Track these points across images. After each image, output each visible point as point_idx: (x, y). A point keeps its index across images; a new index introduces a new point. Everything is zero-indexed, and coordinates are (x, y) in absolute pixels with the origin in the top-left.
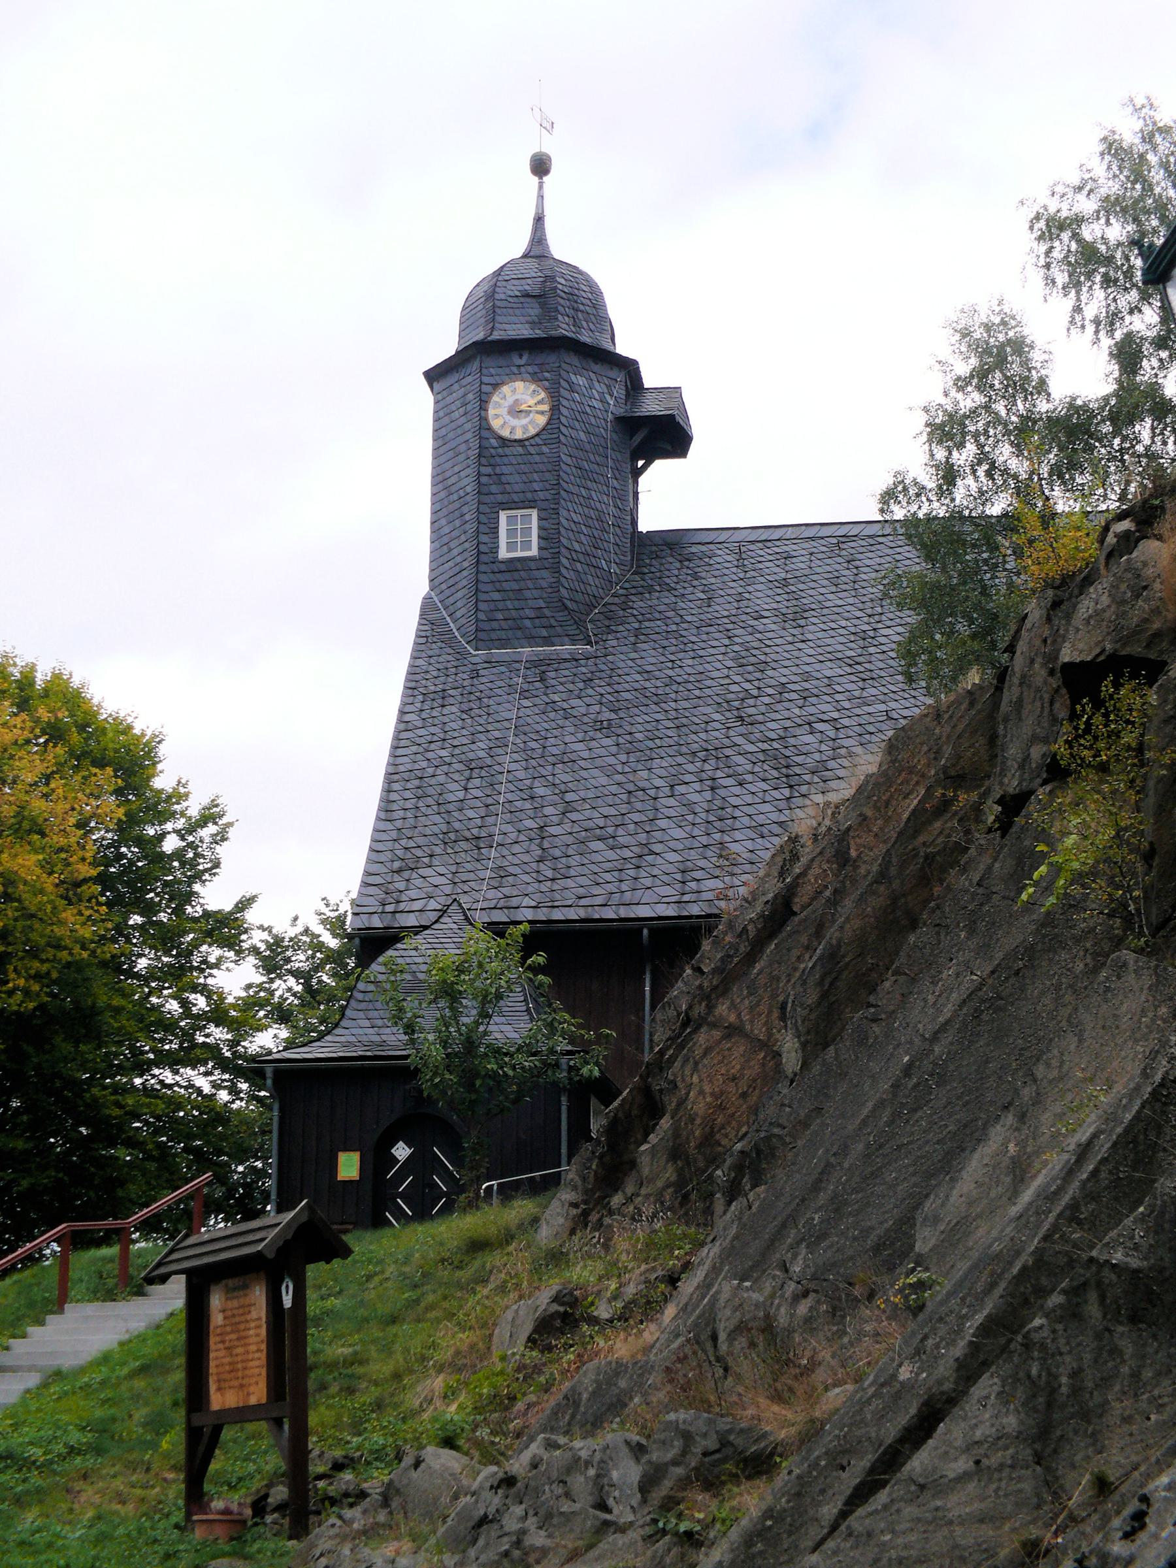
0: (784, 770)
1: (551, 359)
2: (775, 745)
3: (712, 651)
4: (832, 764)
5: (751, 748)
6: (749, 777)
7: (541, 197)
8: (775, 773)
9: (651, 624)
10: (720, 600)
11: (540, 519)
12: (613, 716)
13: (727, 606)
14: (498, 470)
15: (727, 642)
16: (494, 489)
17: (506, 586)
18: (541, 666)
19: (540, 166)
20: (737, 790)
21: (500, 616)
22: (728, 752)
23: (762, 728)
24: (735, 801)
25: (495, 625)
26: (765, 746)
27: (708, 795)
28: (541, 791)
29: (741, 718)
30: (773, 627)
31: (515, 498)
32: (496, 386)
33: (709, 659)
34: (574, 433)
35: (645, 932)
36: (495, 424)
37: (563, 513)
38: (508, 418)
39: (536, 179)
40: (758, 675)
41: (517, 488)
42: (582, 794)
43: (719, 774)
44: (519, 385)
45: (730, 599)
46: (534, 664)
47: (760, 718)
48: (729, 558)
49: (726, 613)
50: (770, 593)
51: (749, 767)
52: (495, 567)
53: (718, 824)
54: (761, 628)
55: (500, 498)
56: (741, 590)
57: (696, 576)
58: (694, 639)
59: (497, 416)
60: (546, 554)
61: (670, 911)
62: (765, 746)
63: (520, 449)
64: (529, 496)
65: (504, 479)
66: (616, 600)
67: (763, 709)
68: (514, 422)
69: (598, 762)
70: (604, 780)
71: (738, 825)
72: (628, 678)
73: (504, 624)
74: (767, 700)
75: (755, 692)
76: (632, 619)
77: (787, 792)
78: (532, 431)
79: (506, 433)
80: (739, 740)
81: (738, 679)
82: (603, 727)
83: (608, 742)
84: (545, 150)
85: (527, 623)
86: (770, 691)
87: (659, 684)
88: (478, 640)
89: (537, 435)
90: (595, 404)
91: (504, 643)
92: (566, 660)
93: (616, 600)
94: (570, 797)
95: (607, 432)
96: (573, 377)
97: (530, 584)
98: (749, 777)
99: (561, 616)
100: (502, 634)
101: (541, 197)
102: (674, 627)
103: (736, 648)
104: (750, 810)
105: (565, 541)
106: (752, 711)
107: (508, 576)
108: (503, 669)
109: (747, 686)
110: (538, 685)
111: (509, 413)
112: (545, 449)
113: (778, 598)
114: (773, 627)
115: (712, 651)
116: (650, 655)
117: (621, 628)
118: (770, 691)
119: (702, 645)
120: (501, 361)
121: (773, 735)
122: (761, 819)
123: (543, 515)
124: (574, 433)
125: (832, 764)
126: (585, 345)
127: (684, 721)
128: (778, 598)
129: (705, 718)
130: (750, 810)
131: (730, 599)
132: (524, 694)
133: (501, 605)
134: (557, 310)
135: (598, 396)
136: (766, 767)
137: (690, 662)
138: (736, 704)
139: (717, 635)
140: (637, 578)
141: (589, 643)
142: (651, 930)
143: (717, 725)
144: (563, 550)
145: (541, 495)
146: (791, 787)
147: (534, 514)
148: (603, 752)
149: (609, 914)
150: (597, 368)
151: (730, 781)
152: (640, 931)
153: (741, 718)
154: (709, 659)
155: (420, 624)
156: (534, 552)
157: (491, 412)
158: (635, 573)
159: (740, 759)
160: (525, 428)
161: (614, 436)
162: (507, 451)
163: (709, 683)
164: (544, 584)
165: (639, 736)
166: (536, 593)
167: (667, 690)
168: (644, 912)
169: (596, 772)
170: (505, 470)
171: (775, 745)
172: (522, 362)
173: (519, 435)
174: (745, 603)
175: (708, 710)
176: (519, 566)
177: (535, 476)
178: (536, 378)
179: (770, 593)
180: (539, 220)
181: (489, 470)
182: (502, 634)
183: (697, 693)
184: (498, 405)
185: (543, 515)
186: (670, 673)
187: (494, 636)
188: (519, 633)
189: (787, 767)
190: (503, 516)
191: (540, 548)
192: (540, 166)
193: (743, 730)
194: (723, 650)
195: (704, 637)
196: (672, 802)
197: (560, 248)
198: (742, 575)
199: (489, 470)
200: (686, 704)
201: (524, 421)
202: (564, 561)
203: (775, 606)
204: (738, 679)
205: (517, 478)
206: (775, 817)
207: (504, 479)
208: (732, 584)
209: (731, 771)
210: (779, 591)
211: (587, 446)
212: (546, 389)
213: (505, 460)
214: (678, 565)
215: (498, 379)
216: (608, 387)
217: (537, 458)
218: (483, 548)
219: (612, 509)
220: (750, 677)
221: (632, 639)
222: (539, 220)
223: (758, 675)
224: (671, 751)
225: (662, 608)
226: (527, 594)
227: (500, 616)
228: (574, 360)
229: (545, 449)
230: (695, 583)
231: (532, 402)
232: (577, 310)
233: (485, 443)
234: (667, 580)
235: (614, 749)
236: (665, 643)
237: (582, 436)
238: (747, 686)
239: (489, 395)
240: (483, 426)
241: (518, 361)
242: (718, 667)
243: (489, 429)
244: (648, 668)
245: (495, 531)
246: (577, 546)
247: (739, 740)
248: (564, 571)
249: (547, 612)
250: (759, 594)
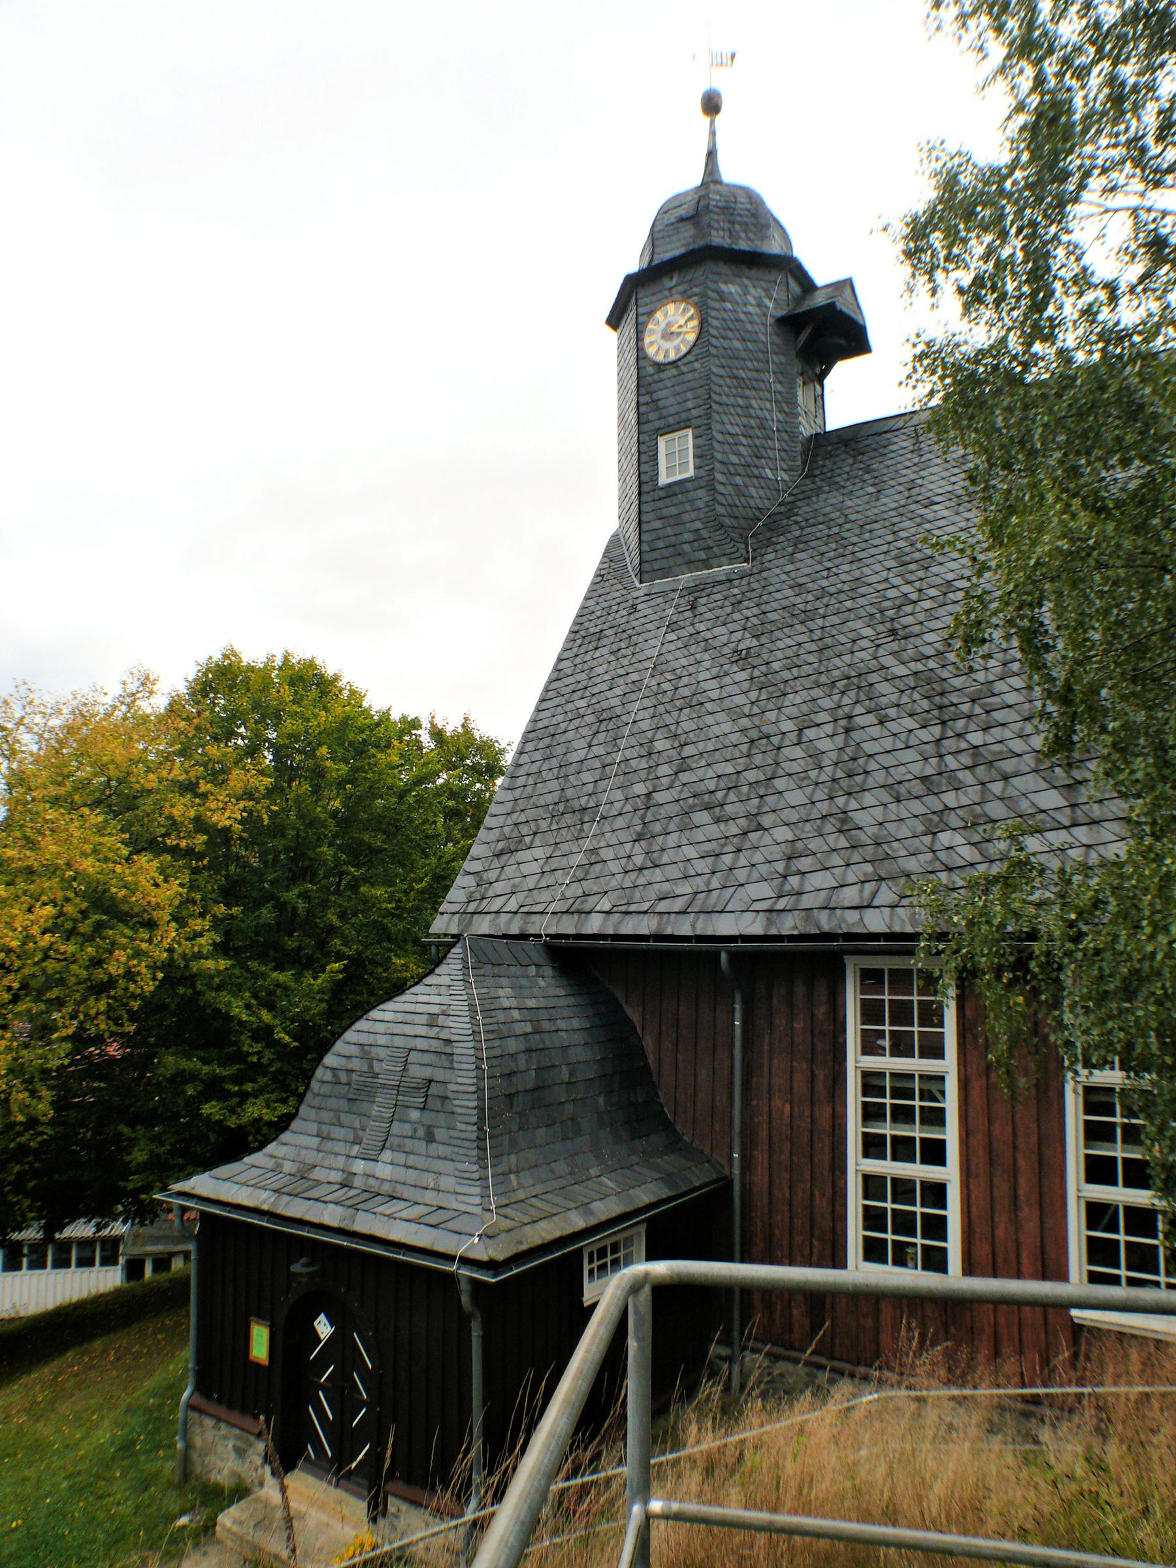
0: (937, 699)
1: (698, 273)
2: (931, 664)
3: (873, 551)
4: (1000, 686)
5: (901, 670)
6: (892, 712)
7: (713, 134)
8: (925, 704)
9: (814, 529)
10: (891, 491)
11: (695, 437)
12: (755, 642)
13: (897, 497)
14: (655, 397)
15: (890, 538)
16: (652, 416)
17: (665, 512)
18: (695, 591)
19: (711, 105)
20: (875, 731)
21: (661, 544)
22: (873, 678)
23: (918, 642)
24: (869, 747)
25: (656, 554)
26: (920, 666)
27: (840, 740)
28: (659, 745)
29: (893, 632)
30: (945, 513)
31: (671, 420)
32: (651, 314)
33: (868, 561)
34: (726, 344)
35: (723, 956)
36: (651, 351)
37: (716, 426)
38: (661, 342)
39: (707, 120)
40: (921, 574)
41: (672, 410)
42: (701, 746)
43: (859, 709)
44: (671, 308)
45: (901, 488)
46: (690, 590)
47: (916, 629)
48: (904, 444)
49: (894, 505)
50: (945, 474)
51: (894, 698)
52: (656, 495)
53: (844, 783)
54: (930, 516)
55: (657, 424)
56: (913, 476)
57: (868, 470)
58: (855, 540)
59: (652, 343)
60: (702, 472)
61: (756, 927)
62: (920, 666)
63: (674, 372)
64: (684, 416)
65: (661, 404)
66: (783, 509)
67: (921, 617)
68: (667, 345)
69: (727, 703)
70: (727, 727)
71: (870, 782)
72: (778, 595)
73: (666, 553)
74: (927, 604)
75: (914, 597)
76: (794, 527)
77: (936, 731)
78: (684, 349)
79: (660, 358)
80: (888, 661)
81: (897, 581)
82: (741, 657)
83: (744, 675)
84: (717, 85)
85: (686, 547)
86: (933, 592)
87: (810, 597)
88: (642, 575)
89: (689, 352)
90: (751, 309)
91: (665, 572)
92: (720, 583)
93: (783, 509)
94: (689, 750)
95: (766, 335)
96: (723, 287)
97: (688, 507)
98: (892, 712)
99: (717, 536)
100: (664, 563)
101: (713, 134)
102: (836, 530)
103: (901, 544)
104: (887, 760)
105: (719, 456)
106: (909, 620)
107: (667, 501)
108: (660, 600)
109: (907, 589)
110: (688, 614)
111: (663, 337)
112: (697, 365)
113: (954, 479)
114: (945, 513)
115: (873, 551)
116: (806, 563)
117: (782, 538)
118: (933, 592)
119: (863, 546)
120: (655, 288)
121: (928, 651)
122: (899, 773)
123: (698, 432)
124: (726, 344)
125: (1000, 686)
126: (743, 252)
127: (829, 641)
128: (954, 479)
129: (852, 635)
130: (887, 760)
131: (901, 488)
132: (672, 627)
133: (661, 533)
134: (709, 226)
135: (757, 302)
136: (916, 696)
137: (847, 567)
138: (890, 613)
139: (879, 533)
140: (807, 481)
141: (746, 560)
142: (732, 955)
143: (865, 643)
144: (717, 466)
145: (695, 413)
146: (943, 723)
147: (689, 432)
148: (734, 689)
149: (684, 927)
150: (753, 273)
151: (871, 719)
152: (717, 955)
153: (893, 632)
154: (868, 561)
155: (602, 563)
156: (690, 473)
157: (647, 340)
158: (806, 477)
159: (884, 688)
160: (677, 349)
161: (777, 340)
162: (663, 375)
163: (863, 590)
164: (700, 504)
165: (776, 666)
166: (694, 515)
167: (818, 604)
168: (725, 926)
169: (722, 717)
170: (661, 394)
171: (931, 664)
172: (674, 282)
173: (672, 356)
174: (916, 491)
175: (858, 624)
176: (676, 488)
177: (689, 395)
178: (686, 297)
179: (945, 474)
180: (711, 155)
181: (647, 398)
182: (664, 563)
183: (849, 604)
184: (653, 332)
185: (698, 432)
186: (824, 583)
187: (656, 565)
188: (679, 560)
189: (942, 694)
190: (662, 442)
191: (696, 468)
192: (711, 105)
193: (895, 646)
194: (885, 548)
195: (867, 536)
196: (798, 752)
197: (730, 174)
198: (916, 460)
199: (647, 398)
200: (835, 620)
201: (677, 341)
202: (719, 476)
203: (949, 488)
204: (897, 581)
205: (672, 400)
206: (916, 769)
207: (661, 404)
208: (905, 472)
209: (872, 705)
210: (956, 471)
211: (744, 355)
212: (695, 305)
213: (661, 385)
214: (851, 461)
215: (651, 307)
216: (767, 290)
217: (689, 376)
218: (644, 478)
219: (776, 416)
220: (910, 577)
221: (790, 550)
222: (711, 155)
223: (921, 574)
224: (807, 683)
225: (828, 509)
226: (686, 517)
227: (661, 544)
228: (723, 268)
229: (697, 365)
230: (867, 476)
231: (682, 322)
232: (733, 223)
233: (642, 373)
234: (838, 479)
235: (746, 685)
236: (824, 549)
237: (737, 344)
238: (907, 589)
239: (645, 324)
240: (641, 355)
241: (669, 283)
242: (877, 570)
243: (646, 357)
244: (801, 580)
245: (655, 457)
246: (735, 459)
247: (888, 661)
248: (720, 488)
249: (704, 533)
250: (933, 478)
